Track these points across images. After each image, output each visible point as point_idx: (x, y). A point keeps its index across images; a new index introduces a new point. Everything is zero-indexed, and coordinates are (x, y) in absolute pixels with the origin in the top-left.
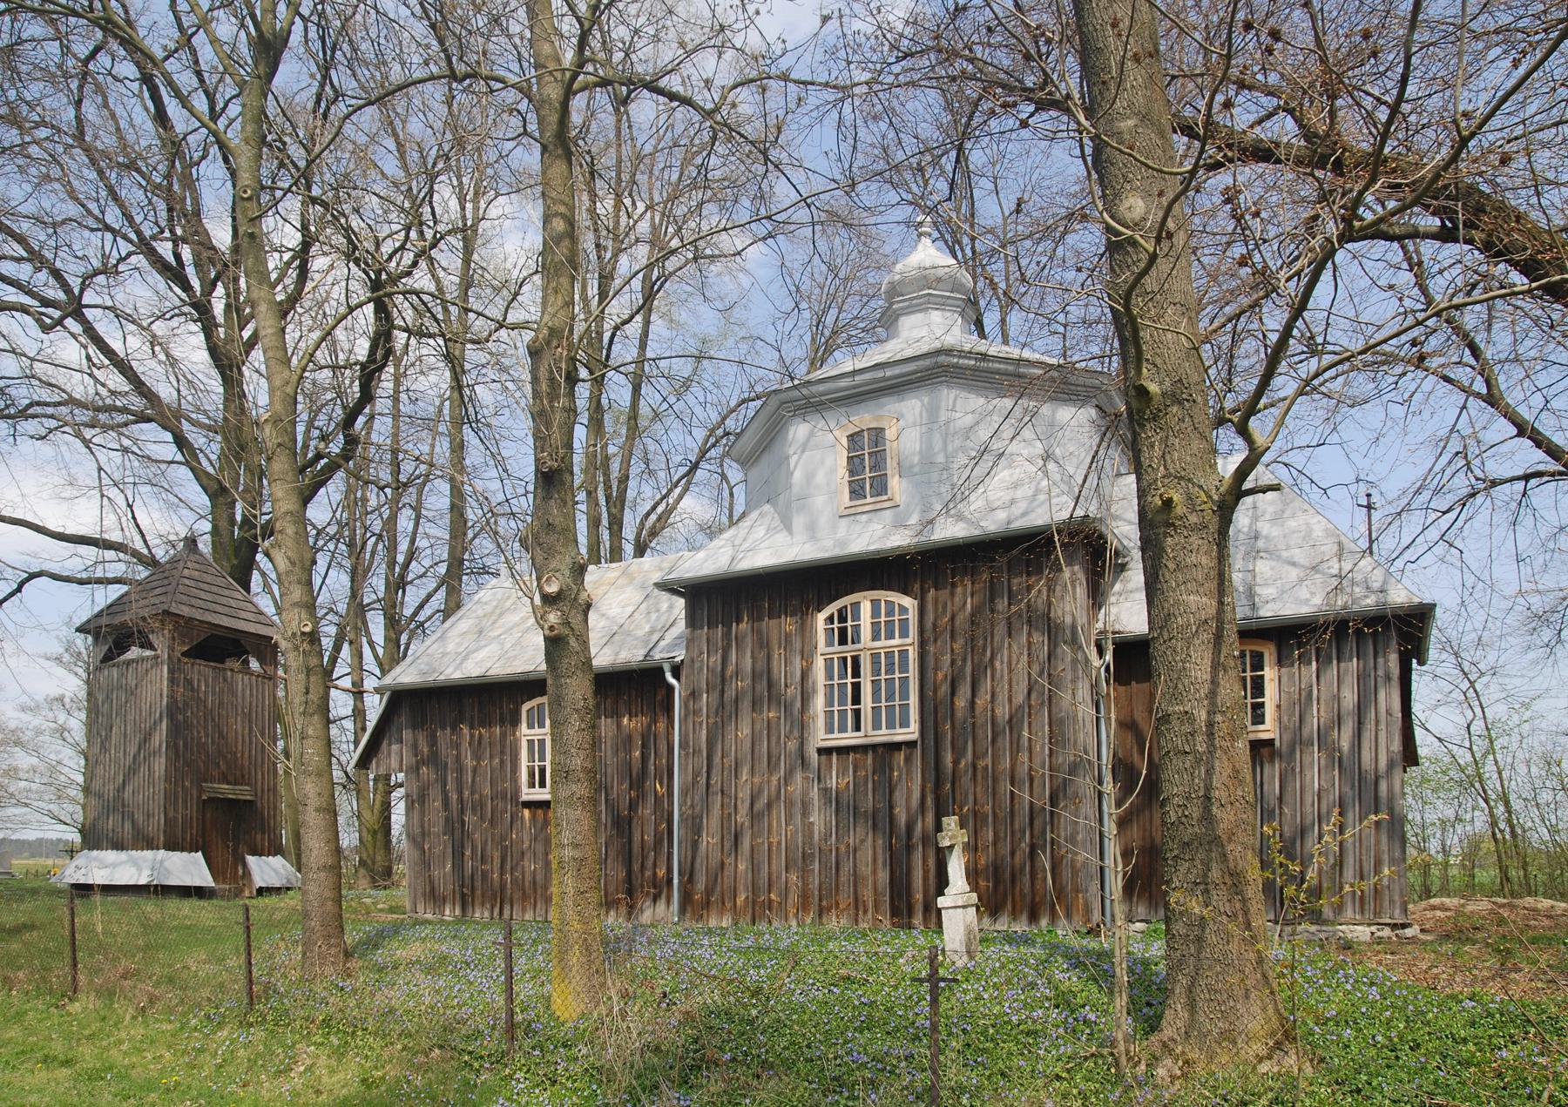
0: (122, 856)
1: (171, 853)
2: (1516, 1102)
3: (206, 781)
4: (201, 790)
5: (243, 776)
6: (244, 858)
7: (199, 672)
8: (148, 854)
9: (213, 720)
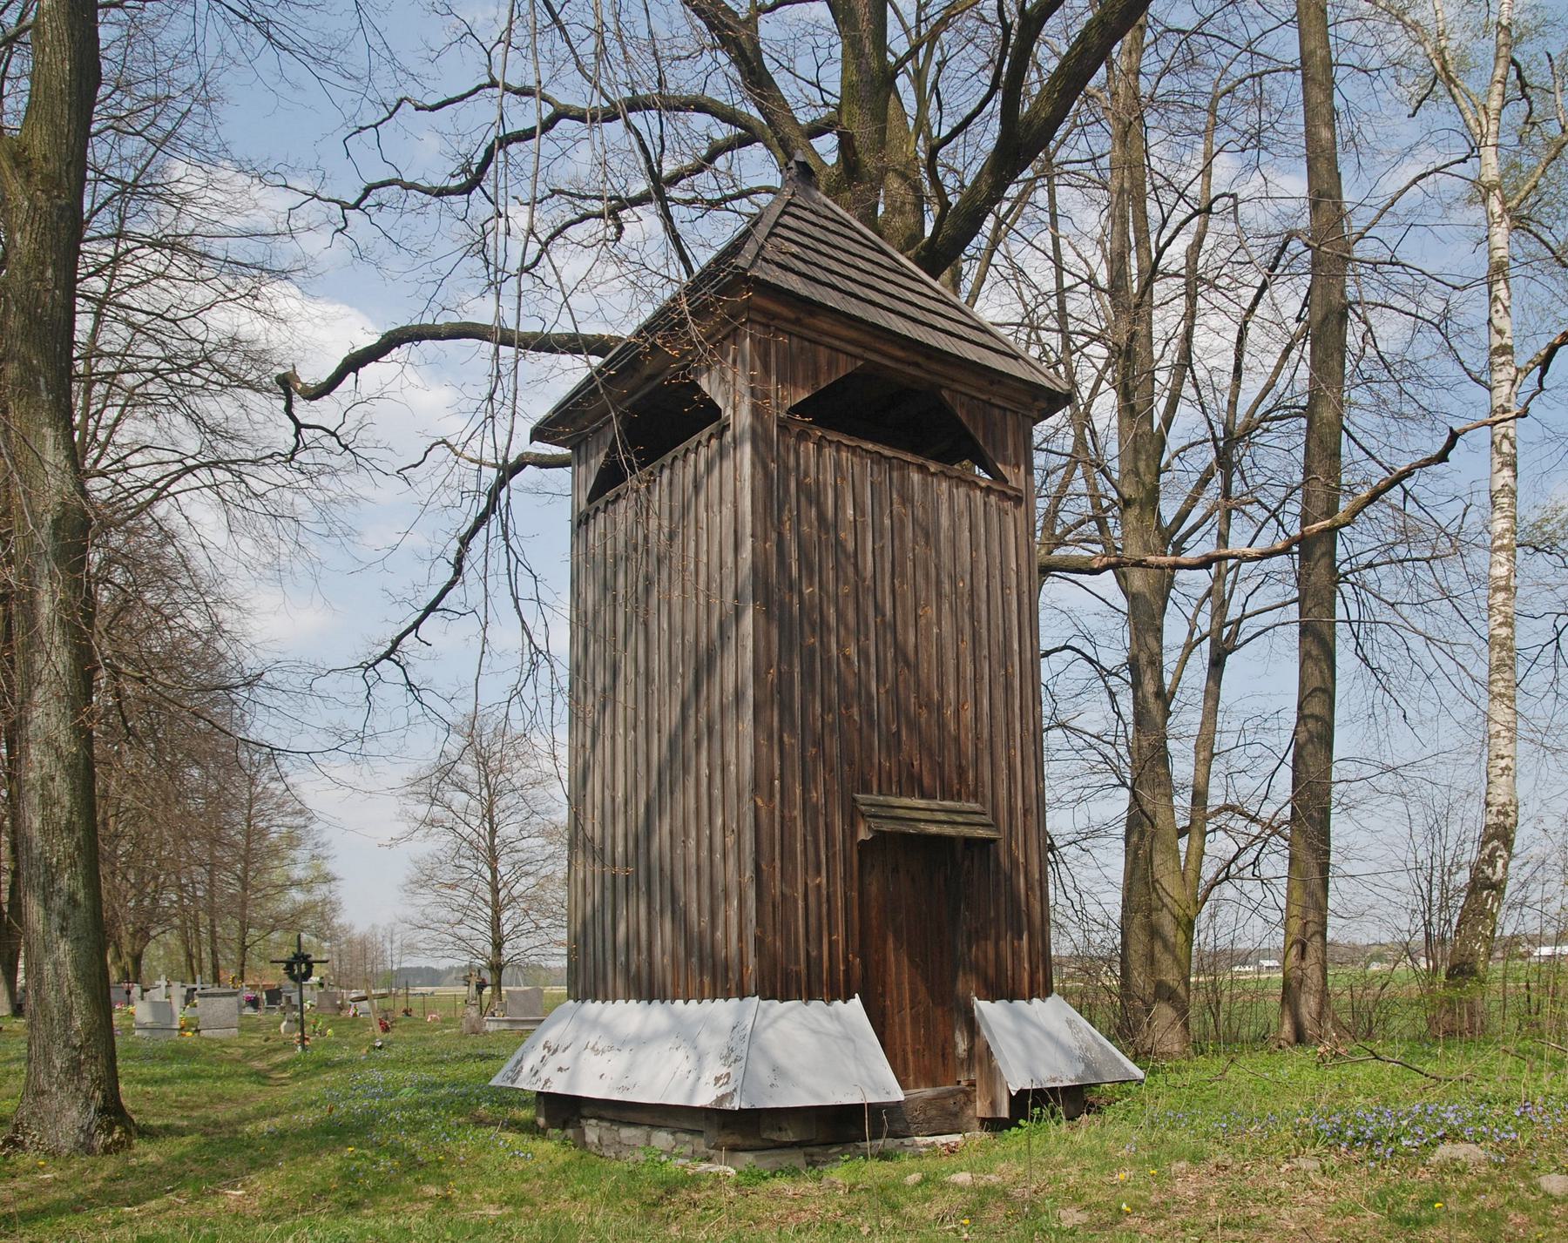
0: (654, 1016)
1: (777, 1006)
2: (1561, 982)
3: (867, 789)
4: (853, 815)
5: (961, 771)
6: (969, 1010)
7: (838, 465)
8: (723, 1010)
9: (879, 609)
